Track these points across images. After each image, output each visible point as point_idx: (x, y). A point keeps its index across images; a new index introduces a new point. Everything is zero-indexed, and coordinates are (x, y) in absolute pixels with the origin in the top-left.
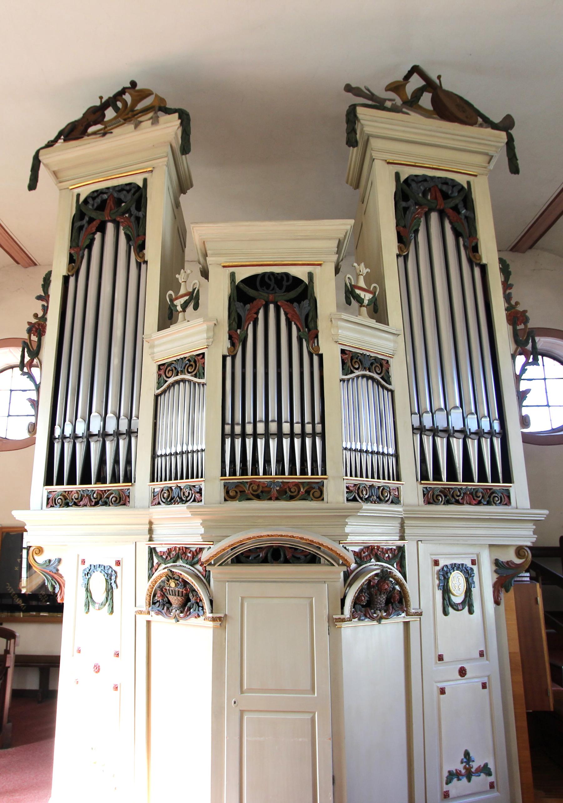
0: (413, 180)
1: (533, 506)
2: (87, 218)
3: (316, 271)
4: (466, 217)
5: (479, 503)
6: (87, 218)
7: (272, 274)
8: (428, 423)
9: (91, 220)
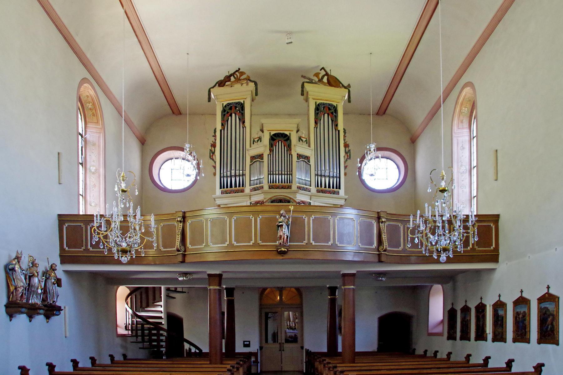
0: (320, 104)
1: (345, 195)
2: (226, 112)
3: (292, 133)
4: (335, 116)
5: (331, 194)
6: (226, 112)
7: (280, 133)
8: (319, 173)
9: (228, 113)
